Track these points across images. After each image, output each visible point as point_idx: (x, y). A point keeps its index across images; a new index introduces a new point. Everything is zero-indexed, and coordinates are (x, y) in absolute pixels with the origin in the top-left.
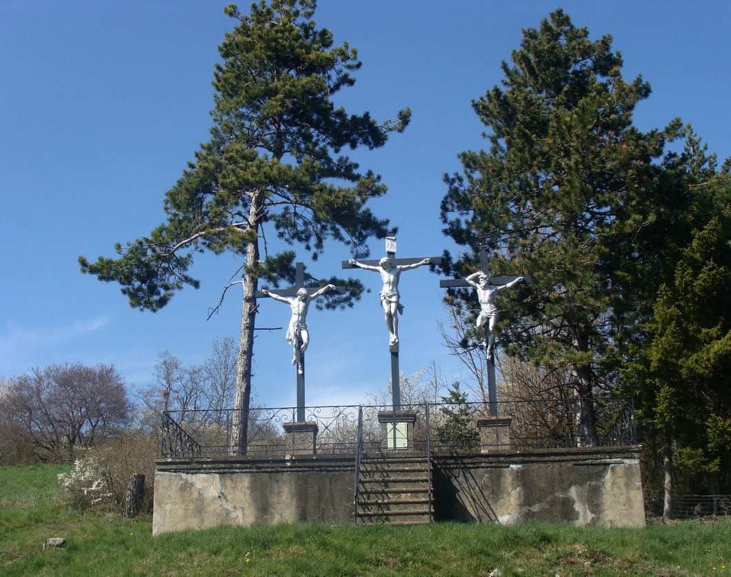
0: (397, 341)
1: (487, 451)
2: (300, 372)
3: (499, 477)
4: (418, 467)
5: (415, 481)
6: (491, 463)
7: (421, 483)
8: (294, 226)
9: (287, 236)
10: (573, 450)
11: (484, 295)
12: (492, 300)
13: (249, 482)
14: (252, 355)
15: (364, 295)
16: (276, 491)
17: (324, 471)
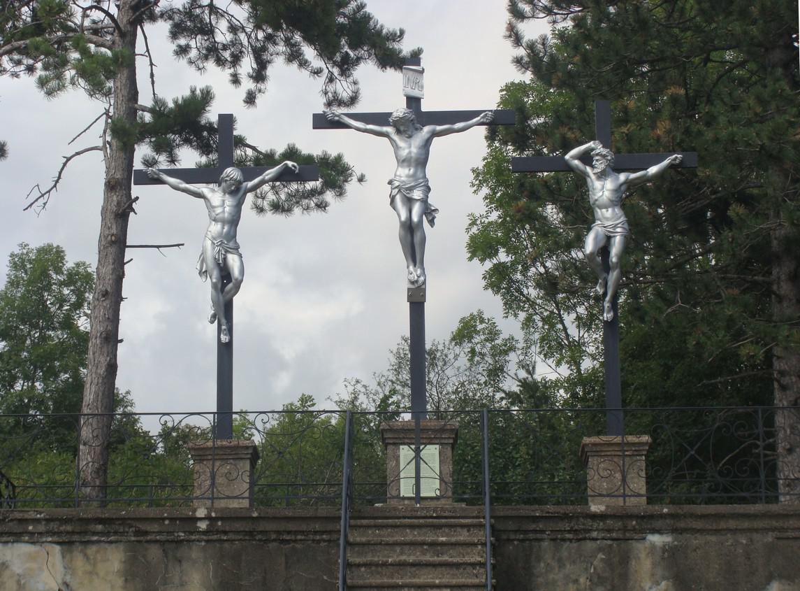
0: (422, 279)
1: (603, 508)
2: (224, 338)
3: (625, 559)
4: (463, 536)
5: (457, 566)
6: (609, 531)
7: (469, 569)
8: (208, 31)
9: (193, 53)
10: (774, 508)
11: (603, 189)
12: (626, 199)
13: (121, 562)
14: (122, 299)
15: (351, 187)
16: (176, 580)
17: (274, 540)
